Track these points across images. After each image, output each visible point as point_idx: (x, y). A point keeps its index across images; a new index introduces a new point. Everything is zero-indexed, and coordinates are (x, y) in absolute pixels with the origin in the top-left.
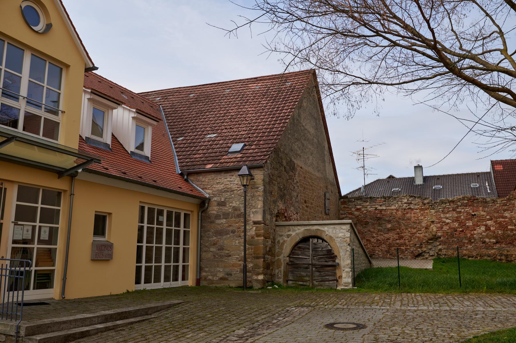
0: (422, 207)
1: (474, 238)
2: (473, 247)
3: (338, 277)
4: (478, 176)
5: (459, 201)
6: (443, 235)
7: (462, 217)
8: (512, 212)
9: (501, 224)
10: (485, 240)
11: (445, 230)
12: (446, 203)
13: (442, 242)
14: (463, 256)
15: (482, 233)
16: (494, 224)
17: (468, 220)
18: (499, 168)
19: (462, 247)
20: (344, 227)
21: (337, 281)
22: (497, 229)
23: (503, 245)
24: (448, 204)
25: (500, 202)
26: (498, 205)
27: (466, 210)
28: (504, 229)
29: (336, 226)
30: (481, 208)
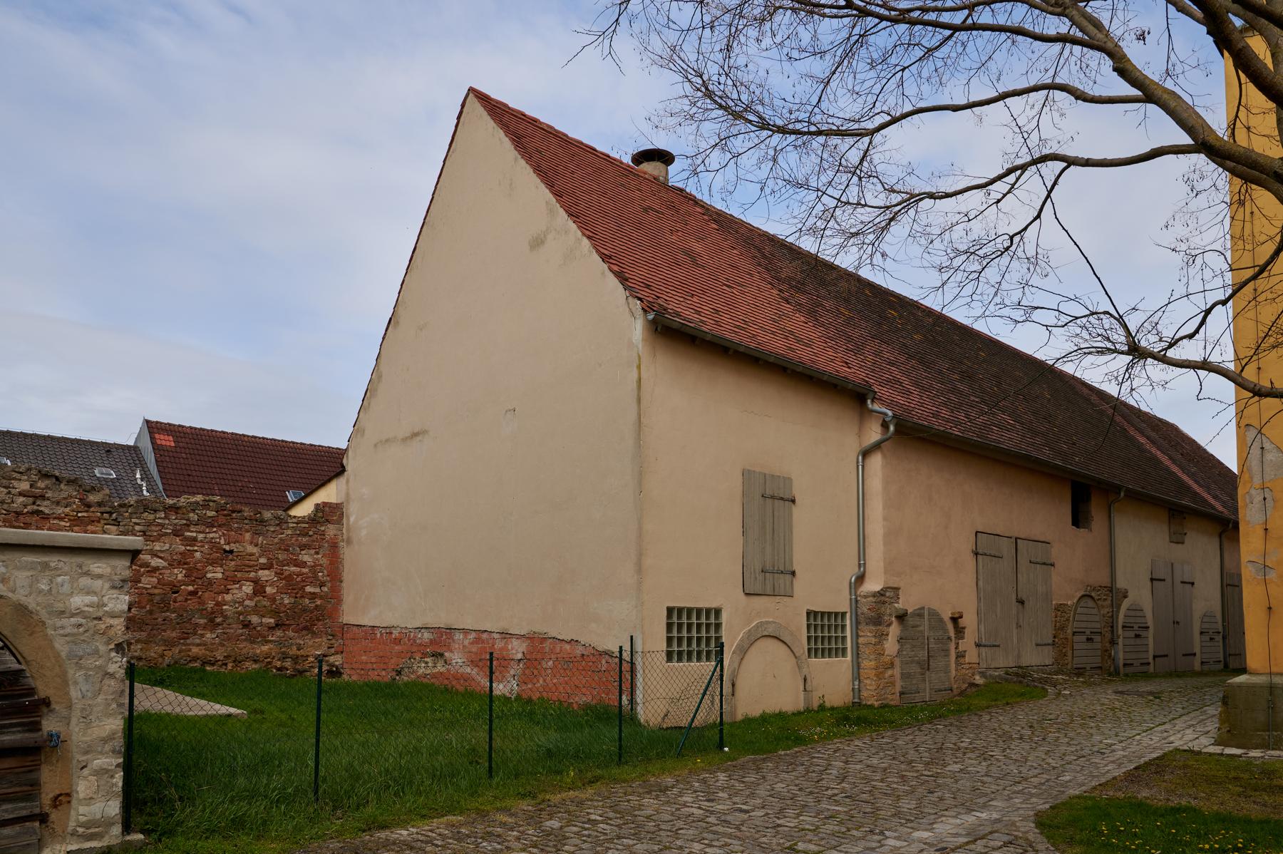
0: (78, 512)
1: (222, 613)
2: (217, 637)
3: (46, 798)
4: (108, 451)
5: (193, 511)
6: (139, 602)
7: (198, 555)
8: (317, 553)
9: (292, 580)
10: (249, 618)
11: (146, 589)
12: (155, 511)
13: (134, 621)
14: (190, 661)
15: (244, 601)
16: (276, 579)
17: (211, 565)
18: (167, 441)
19: (188, 638)
20: (99, 566)
21: (43, 818)
22: (282, 593)
23: (291, 634)
24: (163, 516)
25: (295, 525)
26: (289, 532)
27: (211, 535)
28: (297, 593)
29: (54, 560)
30: (248, 536)
